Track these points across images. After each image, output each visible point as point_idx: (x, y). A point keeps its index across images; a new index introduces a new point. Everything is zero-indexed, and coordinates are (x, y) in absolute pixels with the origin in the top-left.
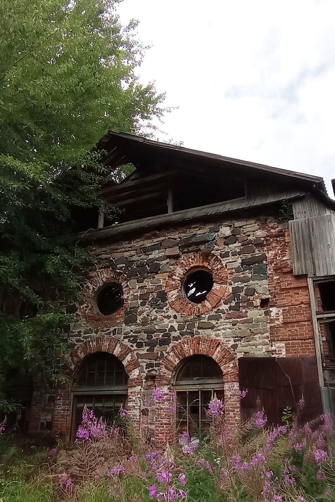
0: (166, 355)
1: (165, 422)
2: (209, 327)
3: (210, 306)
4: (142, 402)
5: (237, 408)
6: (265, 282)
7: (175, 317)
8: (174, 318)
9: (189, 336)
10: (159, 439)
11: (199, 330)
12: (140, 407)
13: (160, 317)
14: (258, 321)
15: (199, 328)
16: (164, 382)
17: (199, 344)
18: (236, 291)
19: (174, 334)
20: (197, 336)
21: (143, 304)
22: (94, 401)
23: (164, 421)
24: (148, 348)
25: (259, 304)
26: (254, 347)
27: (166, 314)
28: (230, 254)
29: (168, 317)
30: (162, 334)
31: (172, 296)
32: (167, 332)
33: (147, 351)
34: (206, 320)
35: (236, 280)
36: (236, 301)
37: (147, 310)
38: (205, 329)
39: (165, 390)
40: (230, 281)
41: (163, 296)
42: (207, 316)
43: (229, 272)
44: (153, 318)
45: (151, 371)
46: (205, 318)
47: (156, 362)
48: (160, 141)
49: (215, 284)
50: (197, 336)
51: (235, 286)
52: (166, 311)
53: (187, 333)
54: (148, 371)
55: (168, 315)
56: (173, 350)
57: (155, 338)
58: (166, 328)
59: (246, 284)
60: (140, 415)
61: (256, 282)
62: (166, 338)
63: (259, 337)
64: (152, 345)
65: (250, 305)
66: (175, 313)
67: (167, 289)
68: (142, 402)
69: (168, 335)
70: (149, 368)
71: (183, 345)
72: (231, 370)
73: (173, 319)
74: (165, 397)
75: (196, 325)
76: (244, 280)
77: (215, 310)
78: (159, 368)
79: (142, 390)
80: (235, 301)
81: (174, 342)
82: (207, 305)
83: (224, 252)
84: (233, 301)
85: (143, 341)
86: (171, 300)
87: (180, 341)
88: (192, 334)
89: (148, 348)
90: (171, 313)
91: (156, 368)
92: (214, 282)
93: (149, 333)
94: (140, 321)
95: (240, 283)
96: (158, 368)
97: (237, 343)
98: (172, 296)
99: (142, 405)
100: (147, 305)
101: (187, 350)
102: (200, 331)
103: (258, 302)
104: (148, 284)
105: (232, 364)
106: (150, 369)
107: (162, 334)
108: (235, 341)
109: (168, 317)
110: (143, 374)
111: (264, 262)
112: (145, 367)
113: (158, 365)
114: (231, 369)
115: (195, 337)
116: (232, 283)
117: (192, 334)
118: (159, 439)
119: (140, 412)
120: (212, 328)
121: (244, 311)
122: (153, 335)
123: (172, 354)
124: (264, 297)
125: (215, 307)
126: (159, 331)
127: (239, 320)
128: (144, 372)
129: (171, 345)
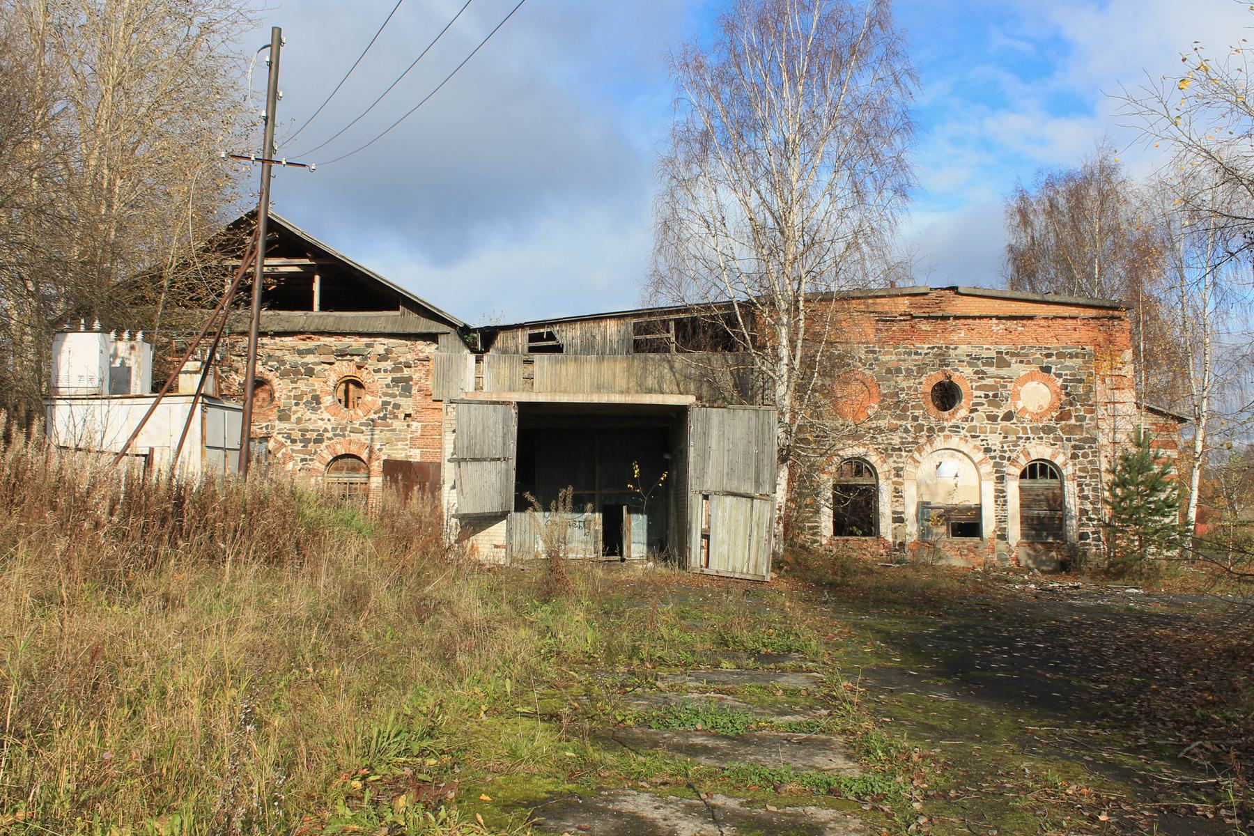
18: (385, 404)
19: (327, 435)
35: (386, 394)
41: (317, 399)
64: (306, 442)
88: (344, 436)
90: (326, 415)
113: (312, 460)
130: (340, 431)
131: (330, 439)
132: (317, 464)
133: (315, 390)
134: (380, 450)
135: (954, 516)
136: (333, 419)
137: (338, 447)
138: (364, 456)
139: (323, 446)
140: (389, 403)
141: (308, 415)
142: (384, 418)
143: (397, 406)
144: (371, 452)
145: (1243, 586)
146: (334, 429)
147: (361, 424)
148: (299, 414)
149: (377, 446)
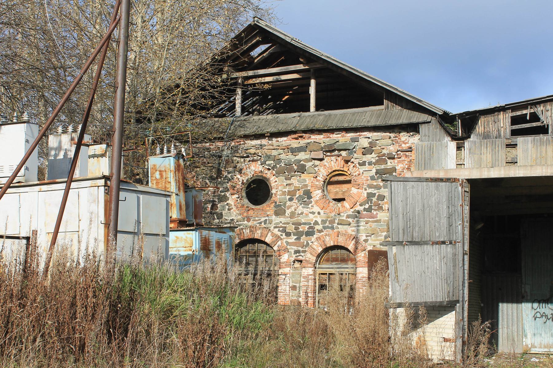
0: (310, 244)
15: (338, 224)
16: (309, 265)
18: (370, 195)
21: (291, 200)
24: (296, 237)
27: (311, 211)
29: (313, 213)
30: (308, 226)
32: (312, 225)
33: (295, 239)
35: (370, 186)
38: (343, 225)
40: (365, 187)
41: (308, 194)
42: (346, 215)
45: (298, 256)
50: (337, 230)
57: (302, 230)
64: (299, 235)
76: (378, 187)
77: (352, 210)
87: (322, 233)
88: (332, 228)
89: (296, 237)
90: (316, 209)
91: (302, 254)
93: (297, 224)
95: (373, 189)
97: (368, 238)
99: (291, 283)
102: (339, 226)
106: (298, 254)
108: (367, 236)
109: (313, 213)
112: (293, 253)
113: (304, 252)
116: (367, 189)
117: (332, 228)
120: (349, 225)
121: (375, 213)
122: (300, 227)
123: (316, 243)
126: (305, 224)
127: (370, 220)
129: (315, 236)
130: (328, 224)
131: (320, 231)
133: (306, 186)
134: (366, 241)
136: (322, 212)
139: (313, 238)
141: (300, 209)
142: (369, 210)
146: (324, 222)
147: (348, 216)
148: (293, 209)
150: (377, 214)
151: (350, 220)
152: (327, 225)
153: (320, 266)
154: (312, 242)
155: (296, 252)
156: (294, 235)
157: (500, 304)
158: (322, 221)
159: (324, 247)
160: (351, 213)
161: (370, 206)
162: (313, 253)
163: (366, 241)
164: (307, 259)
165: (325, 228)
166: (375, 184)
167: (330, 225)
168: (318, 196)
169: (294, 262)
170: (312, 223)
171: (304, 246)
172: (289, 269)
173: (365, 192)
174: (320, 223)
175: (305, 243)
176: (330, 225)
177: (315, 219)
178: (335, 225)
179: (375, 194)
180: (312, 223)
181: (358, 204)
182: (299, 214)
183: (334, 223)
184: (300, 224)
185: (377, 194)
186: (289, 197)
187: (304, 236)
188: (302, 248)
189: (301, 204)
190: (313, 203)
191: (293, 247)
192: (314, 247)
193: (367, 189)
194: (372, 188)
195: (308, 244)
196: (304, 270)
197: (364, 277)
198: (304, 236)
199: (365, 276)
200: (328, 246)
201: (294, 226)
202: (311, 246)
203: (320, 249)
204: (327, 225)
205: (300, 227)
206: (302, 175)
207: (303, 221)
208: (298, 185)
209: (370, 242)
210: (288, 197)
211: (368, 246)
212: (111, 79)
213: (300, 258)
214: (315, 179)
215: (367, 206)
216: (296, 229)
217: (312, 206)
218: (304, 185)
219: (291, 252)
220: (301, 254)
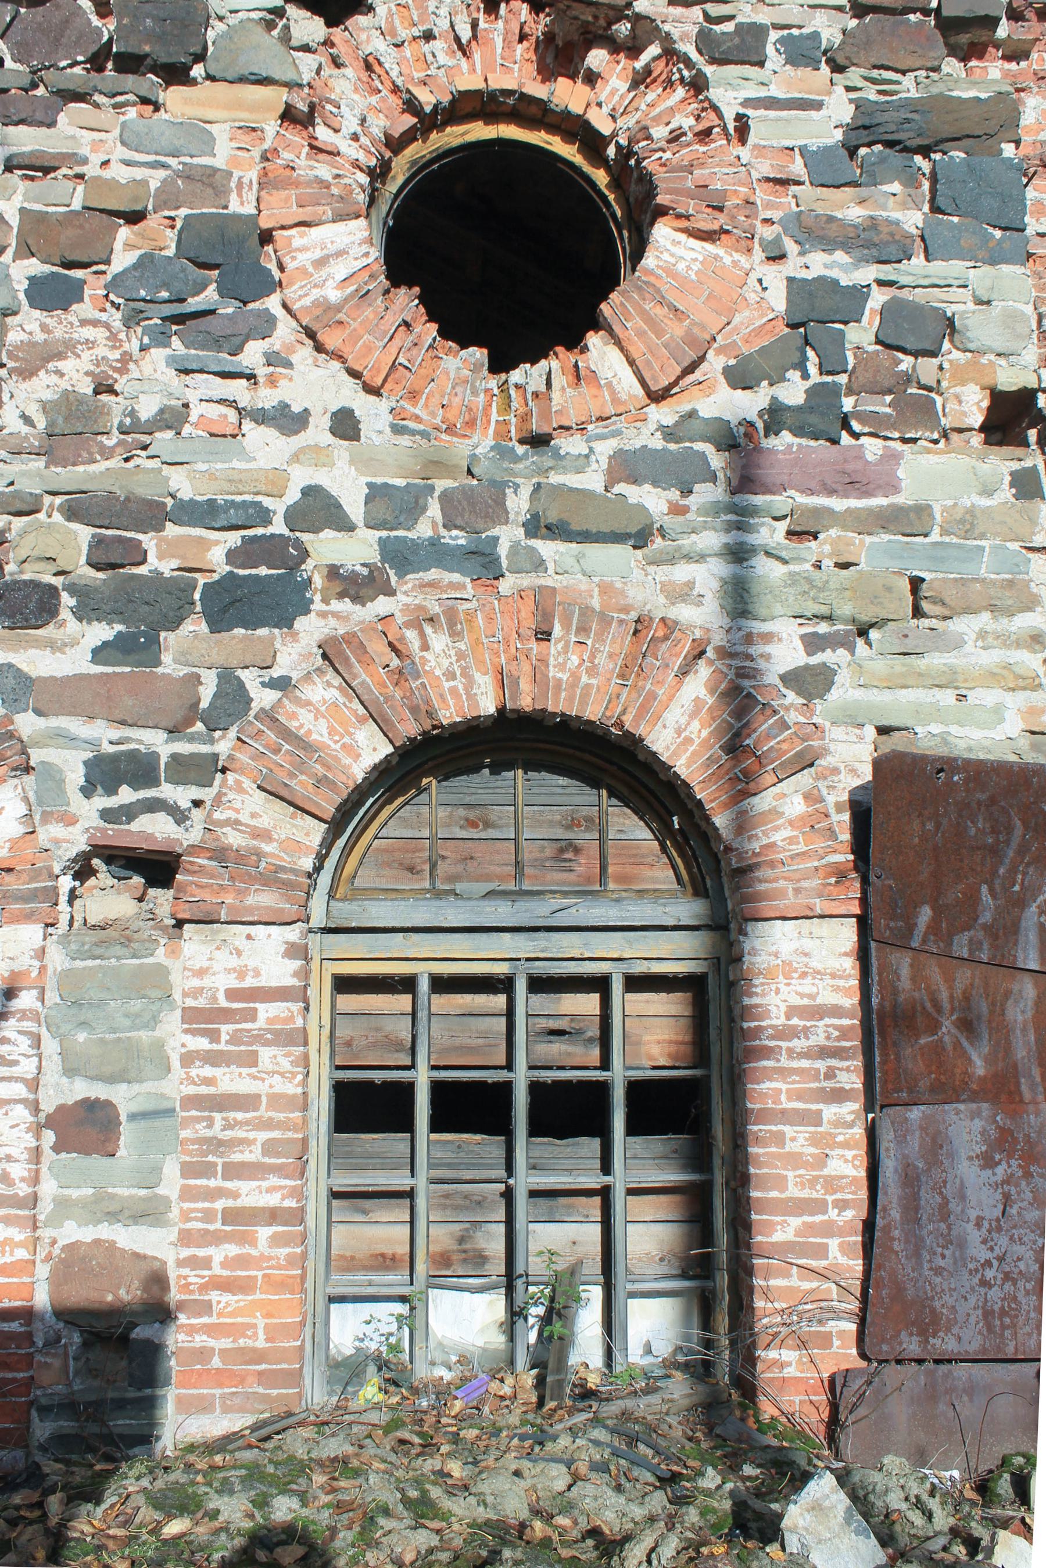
0: (263, 698)
1: (273, 1200)
2: (619, 527)
3: (628, 384)
4: (50, 1046)
5: (839, 1096)
6: (1012, 274)
7: (345, 425)
8: (334, 431)
9: (456, 577)
10: (210, 1330)
11: (537, 544)
12: (34, 1084)
13: (215, 411)
14: (967, 524)
15: (536, 527)
16: (264, 899)
17: (544, 635)
18: (815, 313)
19: (327, 548)
20: (526, 581)
21: (52, 295)
22: (753, 1024)
23: (253, 1194)
24: (102, 632)
25: (977, 419)
26: (948, 697)
27: (267, 398)
28: (770, 50)
29: (288, 420)
30: (234, 538)
31: (321, 263)
32: (278, 527)
33: (99, 654)
34: (593, 480)
35: (816, 233)
36: (815, 377)
37: (90, 344)
38: (586, 537)
39: (266, 955)
40: (768, 233)
41: (234, 257)
42: (605, 449)
43: (765, 168)
44: (147, 410)
45: (128, 813)
46: (585, 469)
47: (184, 748)
48: (664, 994)
49: (662, 232)
50: (526, 581)
51: (809, 275)
52: (262, 372)
53: (436, 553)
54: (106, 815)
55: (284, 407)
56: (330, 654)
57: (167, 567)
58: (267, 502)
59: (886, 272)
60: (37, 1153)
61: (955, 268)
62: (263, 571)
63: (982, 635)
64: (141, 615)
65: (917, 413)
66: (349, 395)
67: (277, 210)
68: (50, 1046)
69: (286, 555)
70: (111, 790)
71: (411, 635)
72: (791, 840)
73: (329, 438)
74: (266, 1011)
75: (519, 503)
76: (878, 244)
77: (664, 414)
78: (206, 794)
79: (57, 959)
80: (805, 376)
81: (336, 605)
82: (605, 373)
83: (729, 27)
84: (794, 375)
85: (58, 581)
86: (316, 293)
87: (382, 605)
88: (483, 563)
89: (102, 632)
90: (316, 385)
91: (181, 795)
92: (662, 211)
93: (119, 520)
94: (27, 420)
95: (840, 256)
96: (195, 792)
97: (827, 657)
98: (321, 263)
99: (53, 1074)
100: (84, 309)
101: (451, 675)
102: (547, 549)
103: (971, 406)
104: (96, 146)
105: (798, 799)
106: (126, 795)
107: (234, 538)
108: (813, 643)
109: (288, 420)
110: (56, 830)
111: (1008, 150)
112: (76, 776)
113: (201, 770)
114: (787, 833)
115: (505, 586)
116: (791, 247)
117: (483, 563)
118: (210, 1330)
119: (37, 1129)
120: (640, 539)
121: (872, 448)
122: (148, 541)
123: (323, 691)
124: (1009, 380)
125: (657, 397)
126: (204, 514)
127: (838, 504)
128: (70, 820)
129: (311, 628)
130: (446, 530)
131: (357, 586)
132: (244, 810)
133: (212, 182)
134: (811, 682)
135: (365, 10)
136: (374, 415)
137: (438, 653)
138: (679, 732)
139: (294, 649)
140: (851, 302)
141: (154, 377)
142: (824, 419)
143: (920, 331)
144: (741, 700)
145: (64, 40)
146: (391, 505)
147: (628, 467)
148: (75, 374)
149: (784, 651)
150: (891, 458)
151: (652, 500)
152: (423, 530)
153: (350, 913)
154: (282, 684)
155: (106, 772)
156: (82, 614)
157: (598, 995)
158: (376, 493)
159: (409, 728)
160: (657, 443)
161: (822, 397)
162: (301, 785)
163: (811, 682)
164: (234, 839)
165: (402, 557)
166: (855, 214)
167: (457, 538)
168: (340, 270)
169: (83, 871)
170: (278, 507)
171: (193, 712)
172: (31, 934)
173: (776, 278)
174: (355, 508)
175: (207, 693)
176: (457, 538)
177: (300, 478)
178: (508, 536)
179: (859, 294)
180: (278, 507)
181: (715, 363)
182: (133, 427)
183: (498, 512)
184: (153, 515)
185: (878, 298)
186: (35, 267)
187: (195, 626)
188: (174, 731)
189: (161, 339)
190: (285, 330)
191: (75, 726)
192: (304, 722)
193: (791, 247)
194: (829, 245)
195: (233, 699)
196: (195, 944)
197: (818, 1012)
198: (195, 626)
199: (828, 997)
200: (449, 715)
201: (84, 533)
202: (269, 716)
203: (371, 749)
204: (423, 530)
205: (148, 541)
206: (173, 96)
207: (183, 485)
208: (120, 173)
209: (843, 692)
210: (24, 270)
211: (837, 733)
212: (250, 1379)
213: (156, 830)
214: (295, 136)
215: (793, 392)
216: (108, 558)
217: (272, 359)
218: (188, 175)
219: (52, 776)
220: (166, 791)
